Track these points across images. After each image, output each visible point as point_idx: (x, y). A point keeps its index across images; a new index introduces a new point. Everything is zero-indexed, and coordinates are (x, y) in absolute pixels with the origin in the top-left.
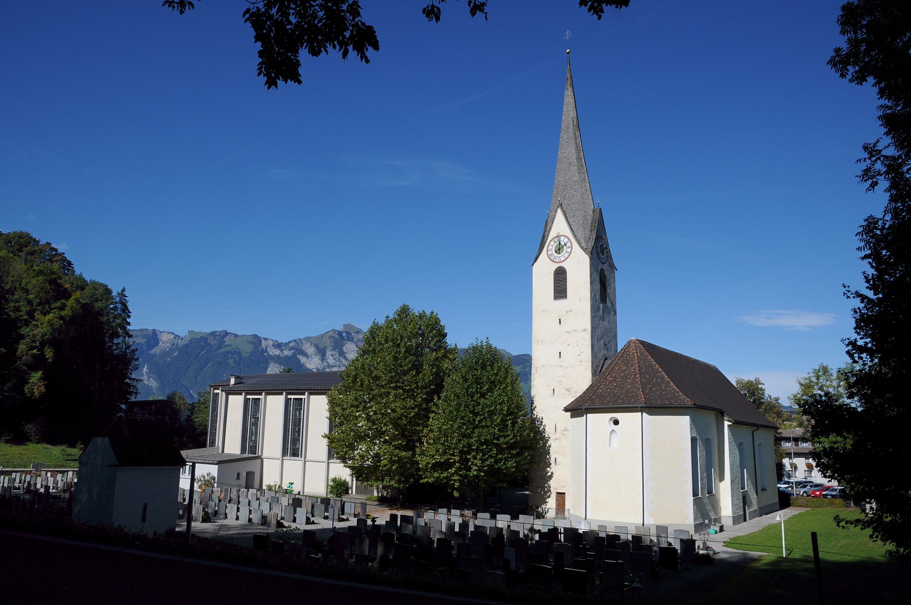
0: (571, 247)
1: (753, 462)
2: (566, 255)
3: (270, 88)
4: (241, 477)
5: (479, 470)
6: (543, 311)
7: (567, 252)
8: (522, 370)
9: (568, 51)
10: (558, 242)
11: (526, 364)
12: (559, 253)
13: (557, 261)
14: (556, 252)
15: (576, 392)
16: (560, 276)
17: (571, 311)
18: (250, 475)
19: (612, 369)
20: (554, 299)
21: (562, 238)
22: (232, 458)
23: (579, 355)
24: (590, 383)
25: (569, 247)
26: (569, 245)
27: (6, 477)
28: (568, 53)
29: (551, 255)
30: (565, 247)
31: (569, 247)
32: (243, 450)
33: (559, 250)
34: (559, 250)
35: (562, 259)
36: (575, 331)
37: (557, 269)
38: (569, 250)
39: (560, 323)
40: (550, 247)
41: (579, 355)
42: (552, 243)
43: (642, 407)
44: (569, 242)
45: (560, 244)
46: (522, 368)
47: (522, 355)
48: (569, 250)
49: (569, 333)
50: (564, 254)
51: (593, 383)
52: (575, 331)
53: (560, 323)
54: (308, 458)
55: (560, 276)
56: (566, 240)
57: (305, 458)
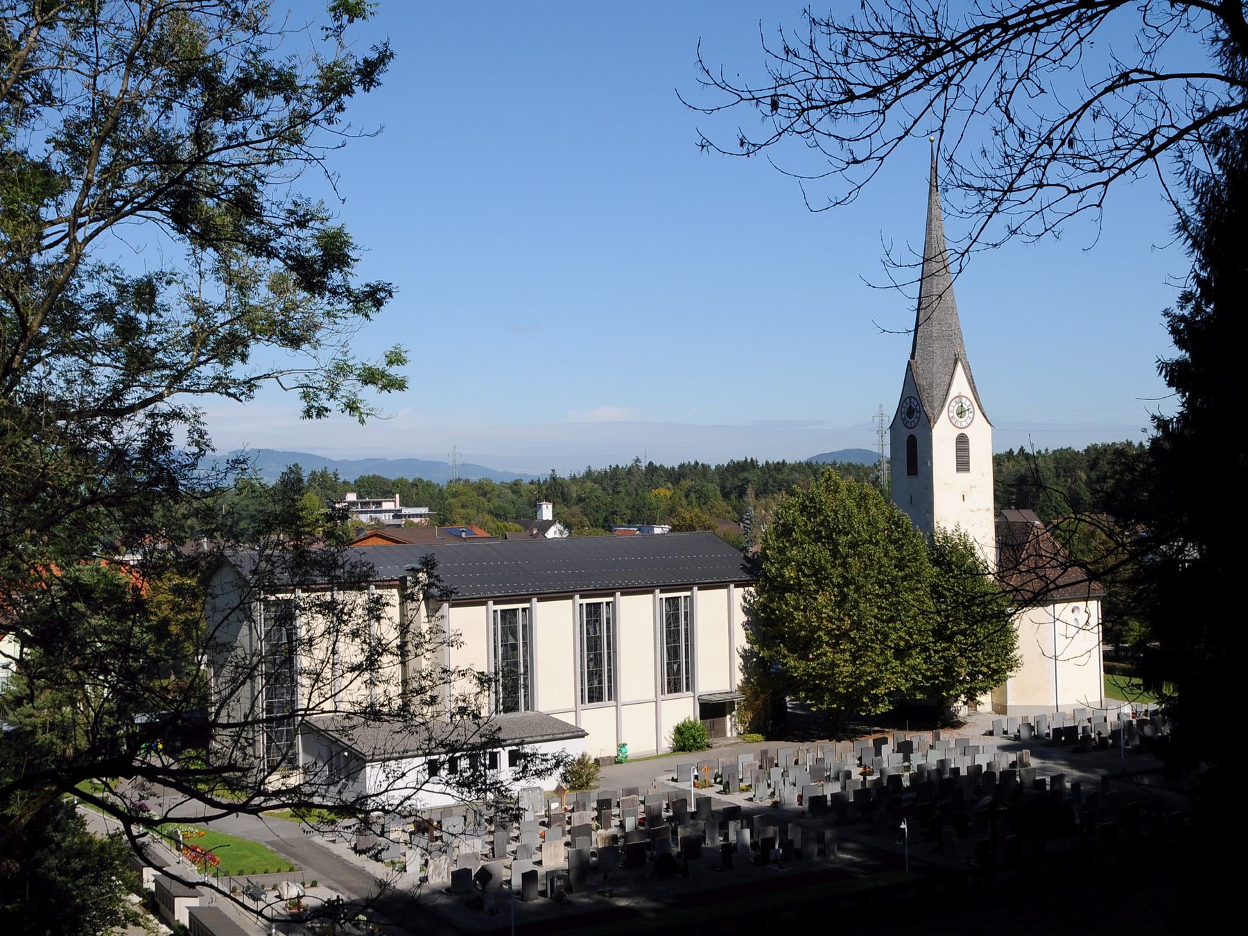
2: (969, 421)
33: (961, 413)
34: (961, 413)
38: (971, 415)
40: (951, 408)
42: (953, 403)
56: (968, 403)
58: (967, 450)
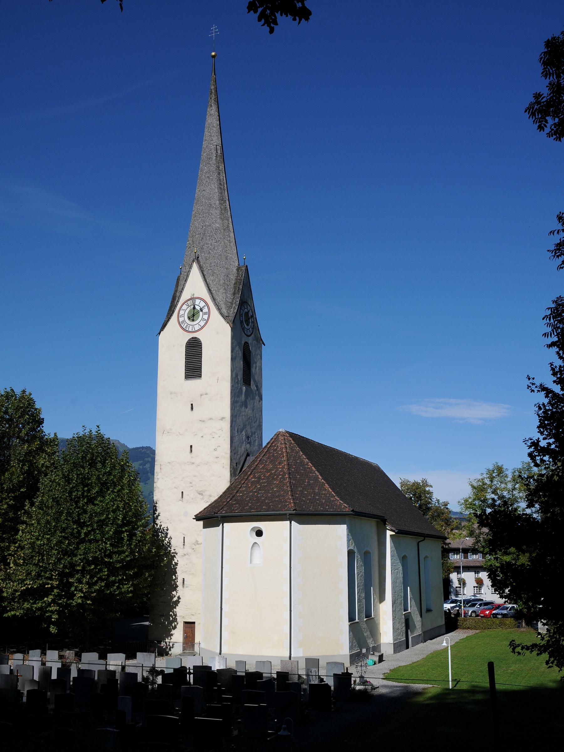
2: (202, 323)
7: (203, 319)
8: (141, 467)
9: (213, 54)
10: (192, 306)
11: (146, 459)
12: (193, 320)
13: (190, 330)
14: (189, 318)
15: (210, 496)
17: (206, 394)
21: (197, 302)
23: (215, 450)
25: (205, 313)
28: (214, 57)
29: (183, 322)
30: (201, 313)
31: (205, 313)
33: (193, 316)
34: (193, 316)
35: (197, 328)
36: (211, 419)
37: (189, 340)
38: (206, 317)
39: (192, 408)
40: (182, 312)
41: (215, 450)
42: (185, 307)
43: (290, 514)
45: (194, 308)
46: (140, 465)
47: (140, 448)
48: (206, 317)
49: (204, 421)
52: (211, 419)
53: (192, 408)
56: (202, 304)
58: (199, 354)
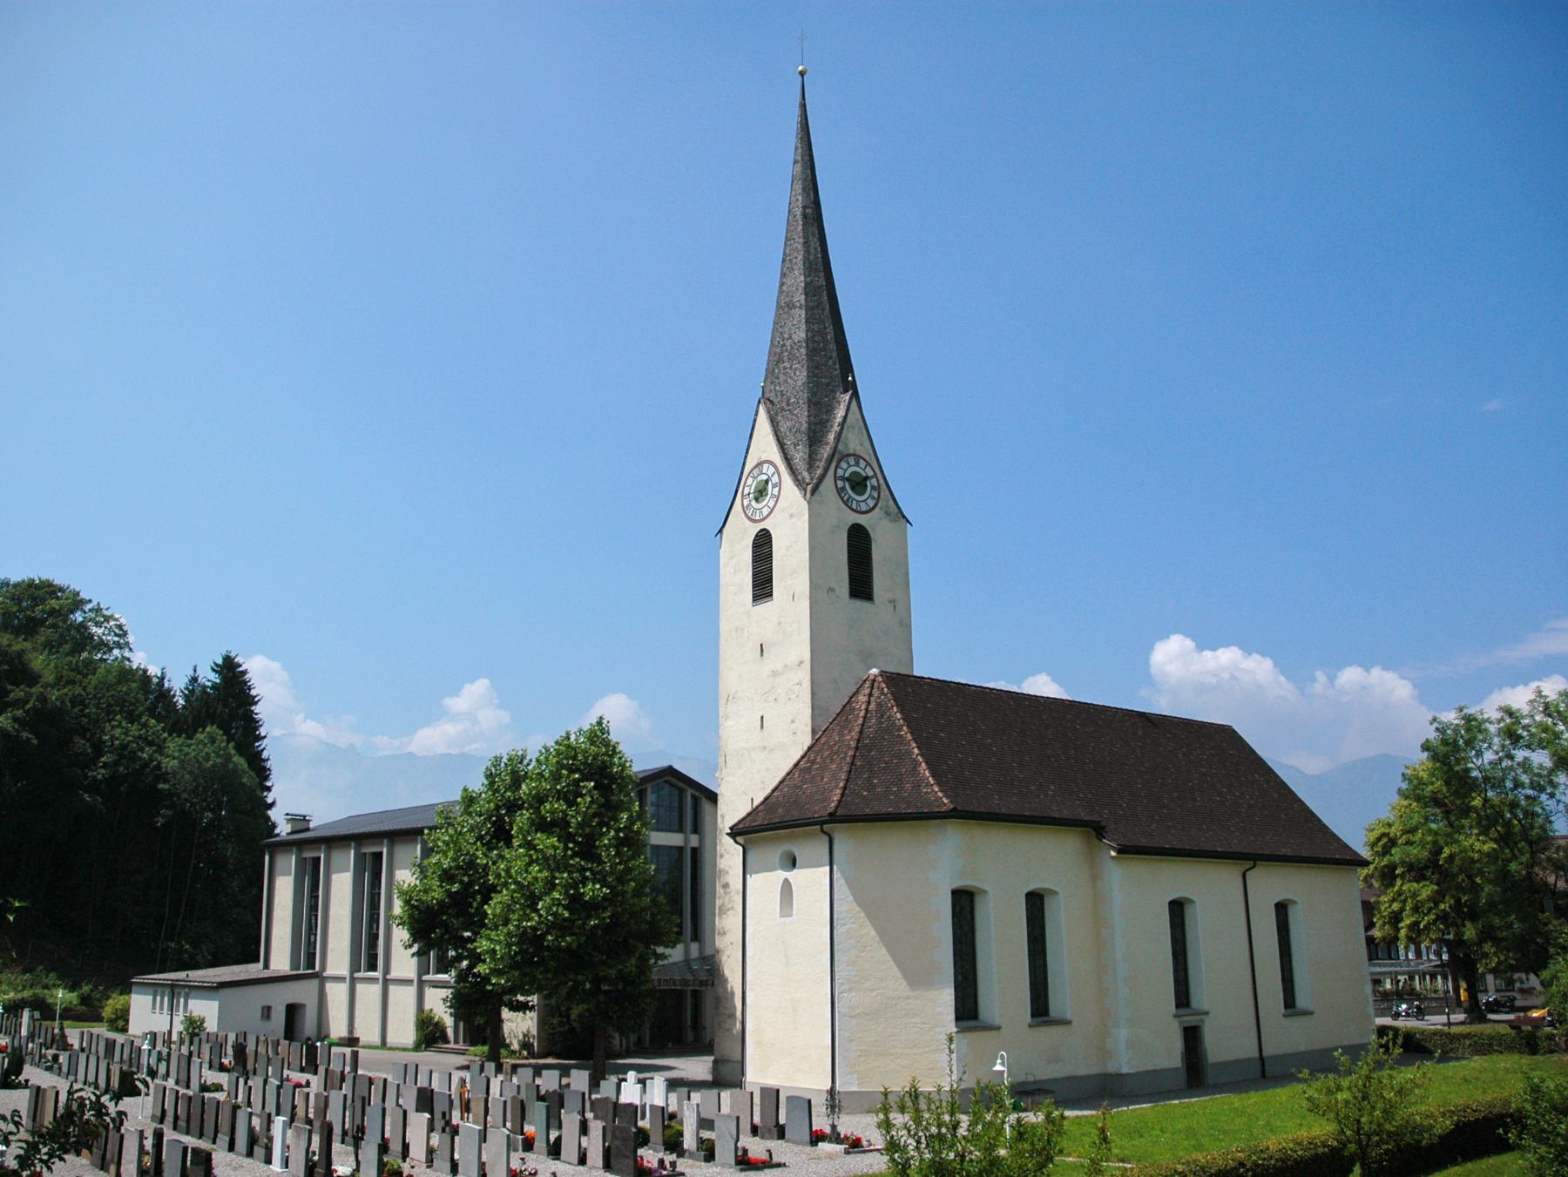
0: (779, 485)
1: (1241, 890)
3: (1051, 890)
4: (273, 1014)
5: (509, 945)
6: (736, 631)
16: (763, 544)
18: (293, 1011)
19: (865, 717)
20: (754, 601)
22: (251, 977)
24: (807, 741)
26: (775, 479)
27: (722, 1094)
32: (295, 964)
34: (761, 493)
38: (776, 491)
44: (776, 475)
50: (768, 501)
51: (815, 742)
54: (394, 974)
55: (763, 544)
56: (772, 469)
57: (387, 970)
